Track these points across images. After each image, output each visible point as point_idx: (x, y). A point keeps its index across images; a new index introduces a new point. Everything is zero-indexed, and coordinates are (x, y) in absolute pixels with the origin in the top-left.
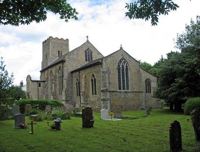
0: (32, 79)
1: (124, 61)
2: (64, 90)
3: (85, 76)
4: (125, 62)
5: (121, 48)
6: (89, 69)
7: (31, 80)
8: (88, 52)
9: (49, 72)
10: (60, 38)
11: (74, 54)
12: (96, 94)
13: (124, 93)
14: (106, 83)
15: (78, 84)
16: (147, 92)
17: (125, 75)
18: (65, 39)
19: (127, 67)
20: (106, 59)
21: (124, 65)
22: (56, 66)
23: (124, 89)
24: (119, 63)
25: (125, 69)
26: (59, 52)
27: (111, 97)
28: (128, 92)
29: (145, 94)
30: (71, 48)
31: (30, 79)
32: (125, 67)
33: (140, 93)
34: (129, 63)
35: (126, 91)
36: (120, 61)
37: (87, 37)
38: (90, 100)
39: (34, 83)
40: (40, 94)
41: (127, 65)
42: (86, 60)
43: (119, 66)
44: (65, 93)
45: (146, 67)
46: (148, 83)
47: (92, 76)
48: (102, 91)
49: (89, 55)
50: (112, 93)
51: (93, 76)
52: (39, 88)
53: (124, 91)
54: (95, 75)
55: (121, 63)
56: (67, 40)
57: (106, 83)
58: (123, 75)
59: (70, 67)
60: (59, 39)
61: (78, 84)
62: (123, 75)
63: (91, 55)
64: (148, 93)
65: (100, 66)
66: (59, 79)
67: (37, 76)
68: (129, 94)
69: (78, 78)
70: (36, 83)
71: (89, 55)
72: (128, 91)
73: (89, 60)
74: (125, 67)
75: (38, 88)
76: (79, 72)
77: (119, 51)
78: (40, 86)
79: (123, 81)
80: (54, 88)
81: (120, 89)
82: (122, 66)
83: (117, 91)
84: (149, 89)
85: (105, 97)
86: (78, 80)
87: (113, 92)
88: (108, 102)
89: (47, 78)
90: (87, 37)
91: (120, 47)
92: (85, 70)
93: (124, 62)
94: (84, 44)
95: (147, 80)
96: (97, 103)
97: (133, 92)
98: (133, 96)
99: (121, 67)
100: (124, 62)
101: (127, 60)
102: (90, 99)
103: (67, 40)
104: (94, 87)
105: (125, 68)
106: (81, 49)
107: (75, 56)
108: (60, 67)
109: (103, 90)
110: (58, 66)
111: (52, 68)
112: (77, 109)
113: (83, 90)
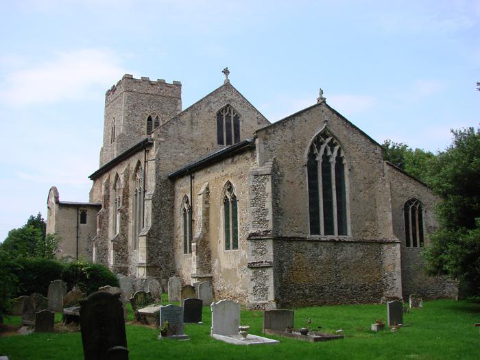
0: (61, 200)
1: (329, 140)
2: (145, 231)
3: (207, 189)
4: (335, 145)
5: (322, 102)
6: (219, 165)
7: (57, 202)
8: (228, 117)
9: (113, 178)
10: (154, 79)
11: (183, 124)
12: (235, 246)
13: (328, 244)
14: (265, 213)
15: (188, 215)
16: (231, 246)
17: (334, 187)
18: (169, 81)
19: (339, 159)
20: (267, 133)
21: (329, 153)
22: (131, 159)
23: (329, 230)
24: (312, 148)
25: (333, 167)
26: (150, 119)
27: (283, 259)
28: (345, 242)
29: (402, 249)
30: (187, 101)
31: (57, 198)
32: (333, 160)
33: (294, 244)
34: (346, 146)
35: (336, 237)
36: (317, 142)
37: (226, 72)
38: (220, 267)
39: (64, 210)
40: (83, 244)
41: (342, 155)
42: (220, 142)
43: (312, 156)
44: (148, 242)
45: (396, 158)
46: (413, 212)
47: (226, 188)
48: (250, 236)
49: (228, 125)
50: (286, 244)
51: (230, 187)
52: (81, 225)
53: (329, 237)
54: (234, 185)
55: (319, 149)
56: (178, 85)
57: (265, 213)
58: (327, 187)
59: (169, 162)
60: (152, 84)
61: (188, 215)
62: (327, 187)
63: (237, 126)
64: (415, 245)
65: (248, 155)
66: (136, 199)
67: (80, 191)
68: (348, 248)
69: (189, 196)
70: (73, 212)
71: (228, 125)
72: (342, 238)
73: (229, 142)
74: (333, 160)
75: (78, 227)
76: (192, 178)
77: (313, 110)
78: (84, 221)
79: (328, 205)
80: (121, 226)
81: (315, 230)
82: (336, 158)
83: (303, 239)
84: (418, 232)
85: (260, 258)
86: (187, 202)
87: (291, 239)
88: (270, 273)
89: (107, 198)
90: (226, 72)
91: (318, 96)
92: (209, 170)
93: (332, 145)
94: (216, 91)
95: (409, 202)
96: (239, 275)
97: (363, 242)
98: (360, 254)
99: (319, 158)
100: (329, 144)
101: (341, 138)
102: (219, 263)
103: (178, 85)
104: (231, 224)
105: (335, 162)
106: (203, 106)
107: (184, 130)
108: (139, 163)
109: (254, 234)
110: (133, 162)
111: (119, 166)
112: (142, 295)
113: (198, 232)
